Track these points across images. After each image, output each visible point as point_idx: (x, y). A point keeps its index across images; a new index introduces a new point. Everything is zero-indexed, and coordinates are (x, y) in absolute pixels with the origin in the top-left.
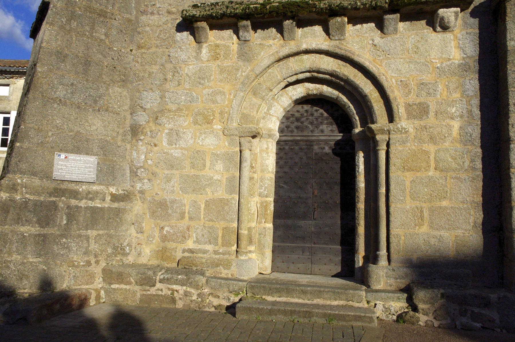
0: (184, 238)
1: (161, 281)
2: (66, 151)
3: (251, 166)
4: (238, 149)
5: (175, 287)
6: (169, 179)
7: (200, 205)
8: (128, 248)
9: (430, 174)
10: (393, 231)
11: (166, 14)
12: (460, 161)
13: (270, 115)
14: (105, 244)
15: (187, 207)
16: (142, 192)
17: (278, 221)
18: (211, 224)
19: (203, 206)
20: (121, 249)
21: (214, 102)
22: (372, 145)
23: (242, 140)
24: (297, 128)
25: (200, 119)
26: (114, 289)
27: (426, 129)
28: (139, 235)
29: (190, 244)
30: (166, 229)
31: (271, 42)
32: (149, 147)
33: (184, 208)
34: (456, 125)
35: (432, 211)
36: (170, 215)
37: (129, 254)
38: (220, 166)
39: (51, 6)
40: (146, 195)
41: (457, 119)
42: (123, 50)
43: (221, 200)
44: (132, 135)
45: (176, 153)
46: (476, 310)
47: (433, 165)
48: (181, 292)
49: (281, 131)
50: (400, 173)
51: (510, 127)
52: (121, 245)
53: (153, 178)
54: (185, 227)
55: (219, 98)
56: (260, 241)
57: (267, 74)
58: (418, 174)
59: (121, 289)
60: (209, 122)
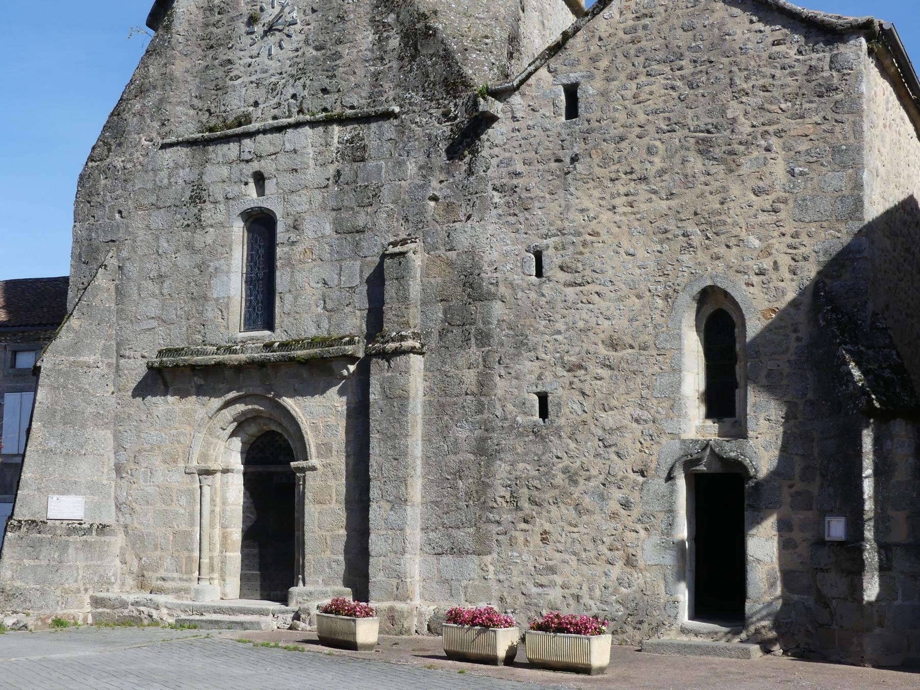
4: (198, 485)
5: (142, 608)
17: (246, 550)
19: (171, 538)
30: (144, 559)
31: (221, 386)
35: (332, 538)
36: (146, 547)
45: (150, 489)
48: (146, 612)
50: (311, 505)
56: (222, 569)
57: (219, 416)
58: (324, 506)
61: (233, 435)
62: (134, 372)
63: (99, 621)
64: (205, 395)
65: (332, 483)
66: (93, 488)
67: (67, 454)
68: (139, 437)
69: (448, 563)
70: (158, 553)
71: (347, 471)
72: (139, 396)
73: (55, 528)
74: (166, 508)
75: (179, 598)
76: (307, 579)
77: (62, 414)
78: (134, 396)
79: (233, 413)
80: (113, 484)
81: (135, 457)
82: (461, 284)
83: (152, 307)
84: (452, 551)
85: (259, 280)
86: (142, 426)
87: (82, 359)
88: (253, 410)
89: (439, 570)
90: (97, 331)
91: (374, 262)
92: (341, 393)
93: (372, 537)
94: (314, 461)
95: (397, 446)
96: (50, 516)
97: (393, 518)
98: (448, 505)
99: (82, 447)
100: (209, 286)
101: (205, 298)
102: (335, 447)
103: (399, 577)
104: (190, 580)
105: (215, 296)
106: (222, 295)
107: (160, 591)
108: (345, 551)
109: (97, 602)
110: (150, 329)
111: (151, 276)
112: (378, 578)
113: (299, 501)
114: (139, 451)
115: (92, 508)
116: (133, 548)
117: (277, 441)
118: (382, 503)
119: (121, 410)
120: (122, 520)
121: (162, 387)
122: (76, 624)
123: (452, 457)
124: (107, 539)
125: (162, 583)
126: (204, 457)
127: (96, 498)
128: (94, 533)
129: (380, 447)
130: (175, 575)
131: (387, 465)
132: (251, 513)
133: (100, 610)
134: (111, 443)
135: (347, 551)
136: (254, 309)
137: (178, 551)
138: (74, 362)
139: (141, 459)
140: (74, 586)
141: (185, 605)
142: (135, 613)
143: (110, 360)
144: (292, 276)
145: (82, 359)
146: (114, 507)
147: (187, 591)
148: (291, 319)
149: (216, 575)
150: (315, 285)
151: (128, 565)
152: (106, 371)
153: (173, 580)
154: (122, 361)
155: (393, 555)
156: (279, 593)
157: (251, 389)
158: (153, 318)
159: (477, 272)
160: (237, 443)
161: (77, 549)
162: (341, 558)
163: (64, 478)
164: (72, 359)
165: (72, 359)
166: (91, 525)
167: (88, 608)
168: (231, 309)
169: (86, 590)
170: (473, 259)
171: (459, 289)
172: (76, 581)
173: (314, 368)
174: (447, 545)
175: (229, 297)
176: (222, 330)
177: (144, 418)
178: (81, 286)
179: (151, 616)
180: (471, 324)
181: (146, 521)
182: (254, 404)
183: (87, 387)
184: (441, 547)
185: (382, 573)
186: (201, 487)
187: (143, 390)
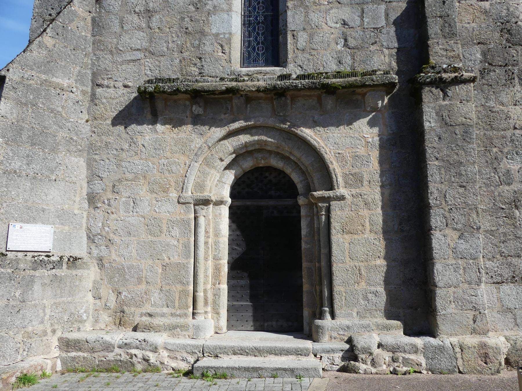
2: (22, 221)
3: (205, 231)
4: (193, 216)
5: (133, 351)
7: (157, 269)
8: (85, 314)
11: (123, 88)
13: (222, 182)
14: (61, 312)
18: (168, 288)
19: (160, 271)
20: (78, 316)
22: (315, 209)
23: (197, 207)
26: (71, 357)
27: (361, 196)
30: (124, 293)
31: (223, 116)
33: (141, 273)
35: (368, 269)
37: (85, 321)
39: (7, 80)
41: (387, 188)
42: (80, 122)
44: (89, 203)
45: (133, 220)
48: (140, 356)
49: (232, 196)
51: (429, 195)
52: (78, 312)
53: (110, 245)
57: (219, 146)
58: (356, 236)
59: (79, 357)
60: (166, 191)
61: (228, 167)
62: (115, 101)
63: (70, 368)
64: (203, 124)
65: (365, 213)
66: (63, 217)
67: (34, 178)
68: (118, 166)
69: (510, 293)
70: (143, 287)
71: (382, 201)
72: (121, 124)
73: (17, 261)
74: (154, 239)
75: (174, 336)
76: (337, 312)
77: (30, 133)
78: (117, 121)
79: (235, 144)
80: (85, 214)
81: (114, 186)
82: (498, 29)
83: (139, 39)
84: (513, 280)
85: (258, 23)
86: (124, 155)
87: (54, 79)
88: (259, 142)
89: (500, 300)
90: (72, 56)
91: (400, 7)
92: (371, 124)
93: (438, 267)
94: (341, 190)
95: (464, 173)
96: (10, 247)
97: (463, 247)
98: (505, 234)
99: (52, 172)
100: (207, 22)
101: (202, 33)
102: (366, 177)
103: (475, 309)
104: (186, 315)
105: (214, 31)
106: (222, 31)
107: (148, 328)
108: (385, 281)
109: (67, 345)
110: (134, 61)
111: (137, 10)
112: (449, 311)
113: (313, 231)
114: (120, 181)
115: (60, 239)
116: (110, 282)
117: (266, 177)
118: (448, 231)
119: (97, 138)
120: (95, 252)
121: (149, 116)
122: (44, 376)
123: (507, 188)
124: (79, 272)
125: (148, 318)
126: (200, 186)
127: (67, 228)
128: (65, 266)
129: (440, 174)
130: (165, 310)
131: (451, 193)
132: (237, 245)
133: (73, 354)
134: (83, 172)
135: (387, 282)
136: (254, 49)
137: (168, 284)
138: (46, 81)
139: (120, 187)
140: (40, 328)
141: (193, 346)
142: (124, 357)
143: (84, 88)
144: (306, 16)
145: (54, 79)
146: (85, 239)
147: (184, 327)
148: (307, 56)
149: (209, 309)
150: (333, 25)
151: (103, 300)
152: (80, 97)
153: (163, 315)
154: (99, 90)
155: (466, 286)
156: (274, 323)
157: (261, 120)
158: (138, 50)
159: (514, 20)
160: (230, 177)
161: (44, 285)
162: (381, 289)
163: (29, 204)
164: (44, 77)
165: (44, 77)
166: (61, 258)
167: (56, 352)
168: (233, 45)
169: (54, 331)
170: (508, 10)
171: (497, 35)
172: (42, 322)
173: (338, 98)
174: (507, 273)
175: (230, 34)
176: (224, 63)
177: (126, 146)
178: (48, 17)
179: (146, 360)
180: (513, 65)
181: (127, 253)
182: (261, 134)
183: (60, 109)
184: (501, 275)
185: (453, 305)
186: (196, 218)
187: (125, 117)
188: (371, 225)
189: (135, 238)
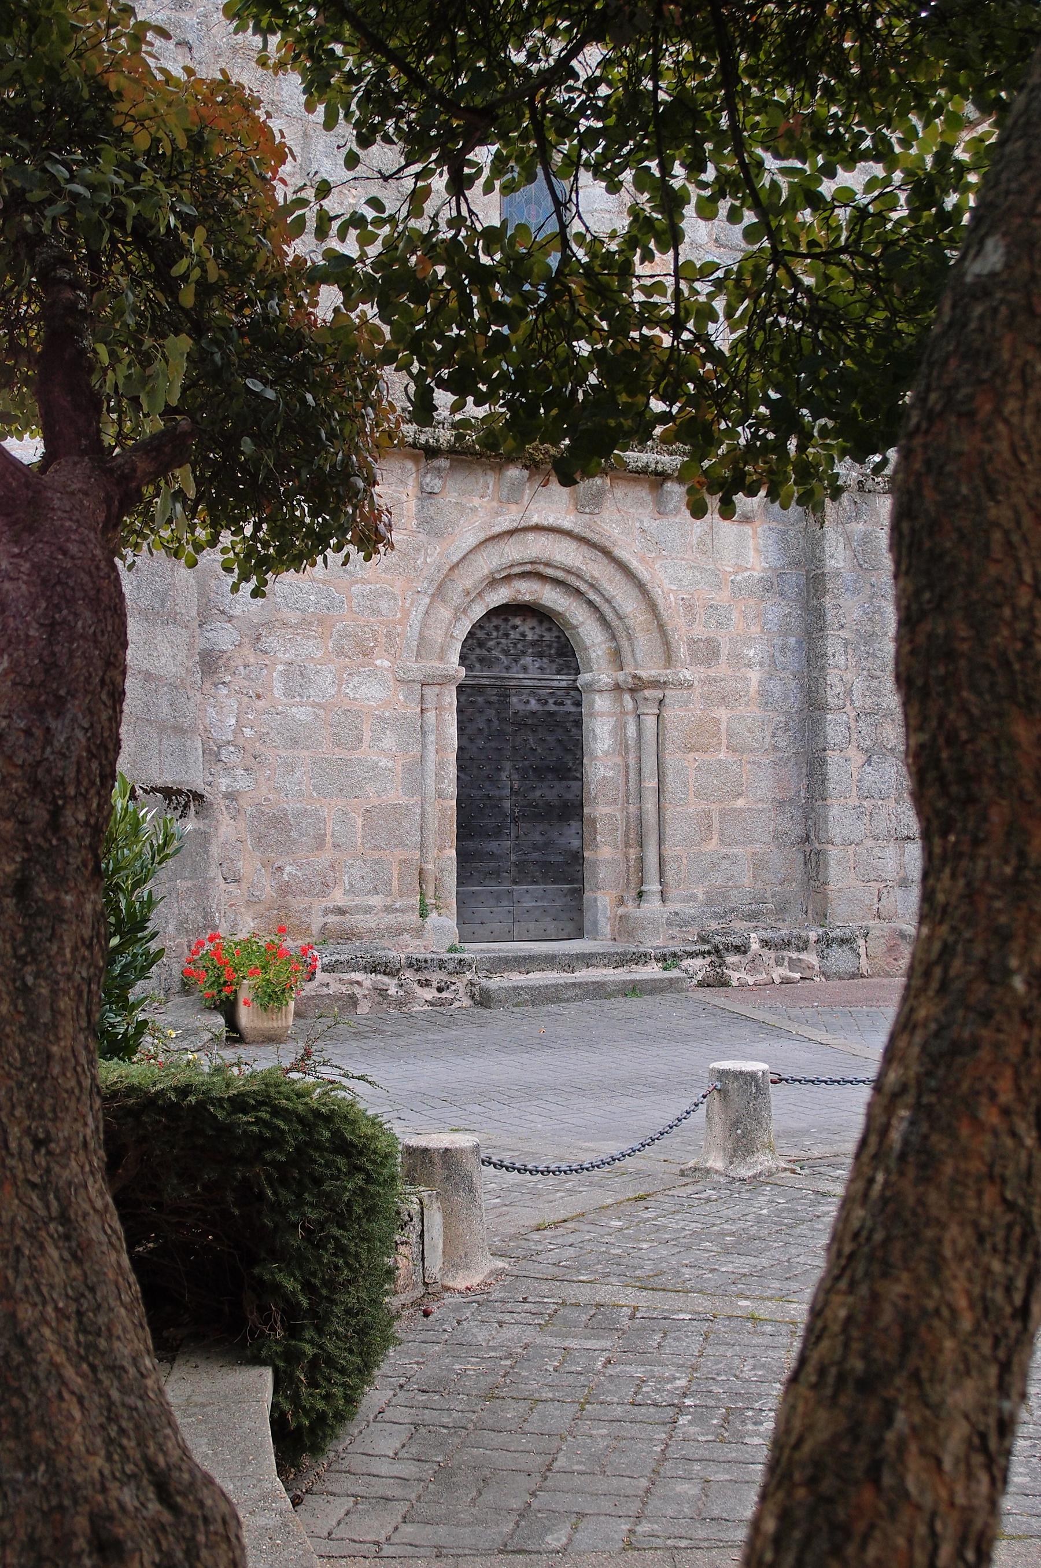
0: (326, 887)
1: (329, 969)
6: (290, 768)
9: (721, 756)
10: (669, 852)
12: (758, 734)
15: (330, 825)
16: (231, 796)
18: (377, 855)
19: (360, 821)
21: (376, 612)
24: (481, 660)
25: (348, 644)
28: (232, 887)
29: (338, 897)
30: (288, 869)
31: (476, 501)
32: (246, 699)
34: (755, 676)
35: (723, 814)
36: (294, 842)
38: (389, 741)
40: (242, 802)
43: (396, 807)
45: (302, 714)
46: (794, 955)
47: (724, 741)
48: (367, 984)
50: (679, 755)
54: (327, 864)
55: (384, 605)
60: (368, 653)
74: (345, 754)
137: (376, 848)
139: (271, 642)
188: (729, 736)
189: (306, 753)
